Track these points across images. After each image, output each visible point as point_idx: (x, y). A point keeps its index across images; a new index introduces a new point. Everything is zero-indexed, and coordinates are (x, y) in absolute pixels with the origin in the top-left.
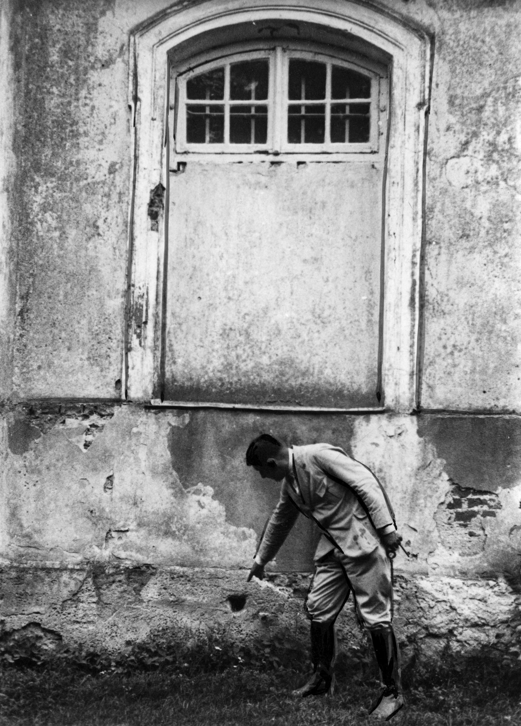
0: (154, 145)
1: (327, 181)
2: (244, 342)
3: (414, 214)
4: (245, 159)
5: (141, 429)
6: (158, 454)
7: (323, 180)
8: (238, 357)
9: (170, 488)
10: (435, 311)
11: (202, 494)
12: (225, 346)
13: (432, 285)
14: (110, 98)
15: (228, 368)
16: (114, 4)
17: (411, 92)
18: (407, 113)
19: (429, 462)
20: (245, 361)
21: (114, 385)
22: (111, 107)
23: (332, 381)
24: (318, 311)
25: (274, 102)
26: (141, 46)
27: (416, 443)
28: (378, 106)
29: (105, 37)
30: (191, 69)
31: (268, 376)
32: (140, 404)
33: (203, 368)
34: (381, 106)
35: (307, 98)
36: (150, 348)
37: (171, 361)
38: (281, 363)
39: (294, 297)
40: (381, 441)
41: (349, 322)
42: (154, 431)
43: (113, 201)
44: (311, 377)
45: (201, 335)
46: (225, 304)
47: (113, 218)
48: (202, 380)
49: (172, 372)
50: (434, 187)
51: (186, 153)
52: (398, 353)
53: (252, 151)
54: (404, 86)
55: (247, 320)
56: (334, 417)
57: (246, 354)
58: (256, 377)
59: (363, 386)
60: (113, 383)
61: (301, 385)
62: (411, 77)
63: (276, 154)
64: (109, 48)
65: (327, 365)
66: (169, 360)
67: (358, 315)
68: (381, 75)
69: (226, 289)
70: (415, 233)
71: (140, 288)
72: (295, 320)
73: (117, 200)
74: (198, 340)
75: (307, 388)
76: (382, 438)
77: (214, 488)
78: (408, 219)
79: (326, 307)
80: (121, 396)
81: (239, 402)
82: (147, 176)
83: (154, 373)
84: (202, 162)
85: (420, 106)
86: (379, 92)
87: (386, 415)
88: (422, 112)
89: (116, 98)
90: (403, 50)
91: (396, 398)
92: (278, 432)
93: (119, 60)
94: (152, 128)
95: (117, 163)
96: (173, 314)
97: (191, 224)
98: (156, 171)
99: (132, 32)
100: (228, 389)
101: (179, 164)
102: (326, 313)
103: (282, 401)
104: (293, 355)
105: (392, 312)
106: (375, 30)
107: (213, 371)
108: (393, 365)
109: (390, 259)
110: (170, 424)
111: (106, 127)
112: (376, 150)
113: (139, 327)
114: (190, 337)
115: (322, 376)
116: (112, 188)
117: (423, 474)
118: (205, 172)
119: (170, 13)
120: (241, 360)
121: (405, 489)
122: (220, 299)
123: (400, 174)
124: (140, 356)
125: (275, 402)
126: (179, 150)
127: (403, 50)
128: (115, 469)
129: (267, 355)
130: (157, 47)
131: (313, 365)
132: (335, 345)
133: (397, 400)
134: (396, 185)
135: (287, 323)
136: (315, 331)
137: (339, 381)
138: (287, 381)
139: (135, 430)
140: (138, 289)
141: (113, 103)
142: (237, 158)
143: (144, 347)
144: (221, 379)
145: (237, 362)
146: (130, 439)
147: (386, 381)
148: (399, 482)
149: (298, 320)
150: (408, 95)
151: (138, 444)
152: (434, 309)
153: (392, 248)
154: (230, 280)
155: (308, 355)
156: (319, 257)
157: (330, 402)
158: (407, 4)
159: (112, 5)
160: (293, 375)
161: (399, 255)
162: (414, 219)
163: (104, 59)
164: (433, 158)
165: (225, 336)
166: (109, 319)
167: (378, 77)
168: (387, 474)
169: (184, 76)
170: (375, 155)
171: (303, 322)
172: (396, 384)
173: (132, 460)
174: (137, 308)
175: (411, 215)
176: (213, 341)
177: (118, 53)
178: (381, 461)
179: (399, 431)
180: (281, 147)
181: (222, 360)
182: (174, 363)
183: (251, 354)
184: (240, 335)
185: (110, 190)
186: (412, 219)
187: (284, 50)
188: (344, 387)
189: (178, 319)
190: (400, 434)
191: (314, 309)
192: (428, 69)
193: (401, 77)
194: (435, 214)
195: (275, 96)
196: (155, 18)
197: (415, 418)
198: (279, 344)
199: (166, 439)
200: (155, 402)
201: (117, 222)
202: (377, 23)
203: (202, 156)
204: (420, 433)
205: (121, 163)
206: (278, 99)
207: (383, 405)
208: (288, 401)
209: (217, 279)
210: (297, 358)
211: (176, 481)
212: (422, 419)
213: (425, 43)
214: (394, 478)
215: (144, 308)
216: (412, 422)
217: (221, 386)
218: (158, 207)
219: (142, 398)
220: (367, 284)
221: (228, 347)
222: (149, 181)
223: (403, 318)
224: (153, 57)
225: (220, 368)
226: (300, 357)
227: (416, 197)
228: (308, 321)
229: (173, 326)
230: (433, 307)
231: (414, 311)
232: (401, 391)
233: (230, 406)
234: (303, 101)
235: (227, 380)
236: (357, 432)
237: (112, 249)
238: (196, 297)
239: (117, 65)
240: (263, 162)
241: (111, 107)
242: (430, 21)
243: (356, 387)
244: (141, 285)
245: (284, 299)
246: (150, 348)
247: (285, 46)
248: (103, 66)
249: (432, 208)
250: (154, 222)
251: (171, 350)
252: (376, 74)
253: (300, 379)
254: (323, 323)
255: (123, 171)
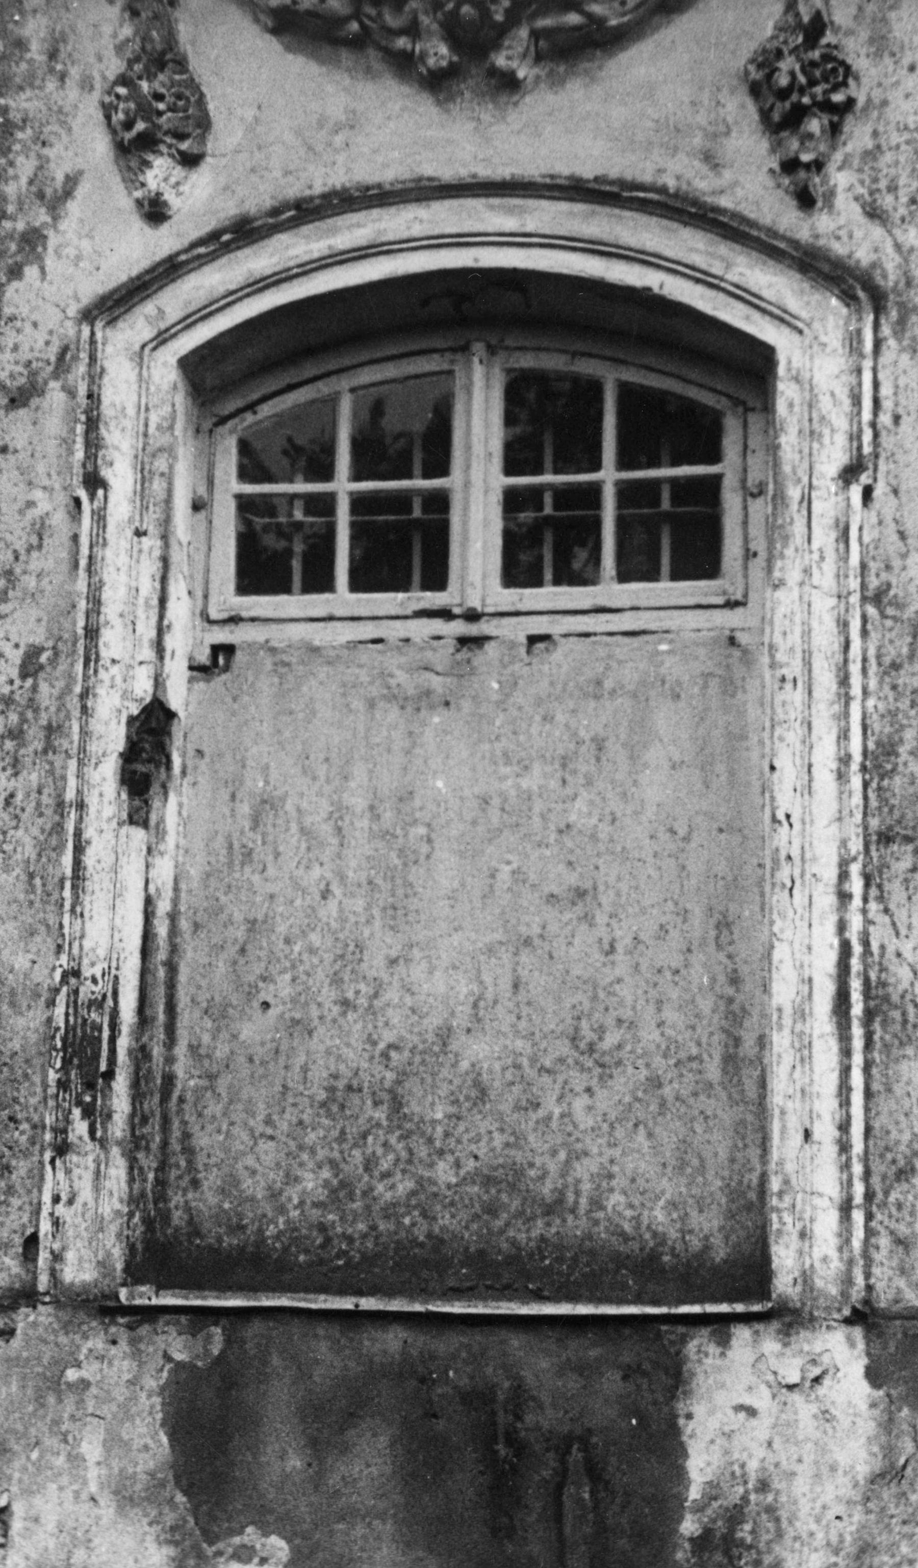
0: (141, 601)
1: (608, 684)
2: (385, 1123)
3: (840, 760)
4: (394, 631)
5: (89, 1372)
6: (137, 1443)
7: (599, 683)
8: (369, 1164)
9: (169, 1542)
10: (909, 1026)
11: (256, 1560)
12: (335, 1133)
13: (899, 955)
14: (30, 483)
15: (342, 1194)
16: (45, 249)
17: (826, 440)
18: (813, 494)
19: (902, 1461)
20: (386, 1175)
21: (20, 1250)
22: (30, 504)
23: (627, 1227)
24: (587, 1034)
25: (467, 484)
26: (109, 349)
27: (863, 1407)
28: (744, 481)
29: (18, 331)
30: (251, 407)
31: (453, 1216)
32: (87, 1300)
33: (274, 1195)
34: (750, 483)
35: (556, 471)
36: (119, 1143)
37: (187, 1179)
38: (488, 1181)
39: (522, 996)
40: (762, 1400)
41: (672, 1062)
42: (127, 1376)
43: (31, 749)
44: (570, 1218)
45: (269, 1106)
46: (334, 1021)
47: (28, 795)
48: (271, 1231)
49: (188, 1208)
50: (894, 687)
51: (234, 620)
52: (807, 1147)
53: (409, 612)
54: (807, 424)
55: (393, 1064)
56: (627, 1332)
57: (391, 1157)
58: (419, 1219)
59: (717, 1241)
60: (18, 1240)
61: (542, 1239)
62: (825, 403)
63: (472, 616)
64: (28, 356)
65: (614, 1183)
66: (180, 1177)
67: (699, 1044)
68: (750, 404)
69: (336, 980)
70: (845, 812)
71: (94, 981)
72: (525, 1062)
73: (39, 745)
74: (260, 1117)
75: (560, 1247)
76: (765, 1392)
77: (289, 1541)
78: (825, 778)
79: (610, 1021)
80: (35, 1278)
81: (372, 1291)
82: (118, 680)
83: (131, 1215)
84: (274, 644)
85: (849, 474)
86: (746, 447)
87: (775, 1325)
88: (856, 493)
89: (46, 482)
90: (801, 332)
91: (804, 1273)
92: (472, 1378)
93: (53, 384)
94: (135, 555)
95: (42, 649)
96: (193, 1049)
97: (245, 809)
98: (144, 667)
99: (88, 315)
100: (341, 1254)
101: (216, 649)
102: (611, 1040)
103: (488, 1287)
104: (519, 1156)
105: (786, 1032)
106: (723, 285)
107: (302, 1203)
108: (794, 1181)
109: (777, 890)
110: (167, 1358)
111: (17, 558)
112: (739, 596)
113: (90, 1086)
114: (238, 1116)
115: (601, 1215)
116: (30, 715)
117: (887, 1494)
118: (284, 670)
119: (187, 262)
120: (376, 1174)
121: (834, 1539)
122: (319, 1005)
123: (799, 655)
124: (92, 1166)
125: (471, 1289)
126: (214, 614)
127: (801, 332)
128: (14, 1489)
129: (450, 1158)
130: (154, 349)
131: (578, 1181)
132: (636, 1125)
133: (806, 1278)
134: (789, 686)
135: (504, 1069)
136: (579, 1089)
137: (649, 1227)
138: (502, 1231)
139: (72, 1375)
140: (88, 983)
141: (38, 495)
142: (368, 631)
143: (103, 1143)
144: (322, 1228)
145: (366, 1178)
146: (60, 1401)
147: (775, 1226)
148: (818, 1520)
149: (533, 1060)
150: (816, 445)
151: (79, 1414)
152: (905, 1022)
153: (783, 854)
154: (349, 957)
155: (562, 1155)
156: (588, 885)
157: (624, 1287)
158: (810, 216)
159: (40, 249)
160: (520, 1214)
161: (802, 875)
162: (841, 777)
163: (16, 384)
164: (890, 611)
165: (335, 1108)
166: (12, 1069)
167: (740, 409)
168: (783, 1499)
169: (230, 424)
170: (740, 610)
171: (548, 1063)
172: (803, 1235)
173: (60, 1461)
174: (83, 1038)
175: (834, 766)
176: (301, 1123)
177: (50, 369)
178: (763, 1460)
179: (816, 1371)
180: (483, 600)
181: (326, 1174)
182: (195, 1184)
183: (404, 1154)
184: (376, 1104)
185: (23, 720)
186: (834, 776)
187: (492, 350)
188: (663, 1243)
189: (206, 1062)
190: (817, 1380)
191: (577, 1029)
192: (867, 377)
193: (797, 401)
194: (900, 760)
195: (468, 467)
196: (147, 278)
197: (858, 1332)
198: (484, 1126)
199: (157, 1400)
200: (131, 1296)
201: (39, 804)
202: (728, 267)
203: (274, 627)
204: (874, 1376)
205: (54, 648)
206: (476, 475)
207: (769, 1299)
208: (507, 1287)
209: (312, 951)
210: (531, 1165)
211: (185, 1521)
212: (880, 1335)
213: (859, 311)
214: (804, 1507)
215: (106, 1034)
216: (852, 1344)
217: (323, 1246)
218: (149, 761)
219: (96, 1283)
220: (722, 956)
221: (342, 1137)
222: (125, 695)
223: (818, 1046)
224: (140, 374)
225: (322, 1195)
226: (538, 1161)
227: (846, 715)
228: (561, 1060)
229: (192, 1083)
230: (904, 1014)
231: (849, 1027)
232: (817, 1253)
233: (346, 1303)
234: (548, 478)
235: (339, 1230)
236: (693, 1374)
237: (24, 877)
238: (256, 1004)
239: (48, 396)
240: (439, 638)
241: (30, 504)
242: (873, 257)
243: (696, 1244)
244: (97, 971)
245: (495, 1002)
246: (119, 1143)
247: (494, 342)
248: (13, 400)
249: (892, 745)
250: (137, 803)
251: (189, 1151)
252: (737, 402)
253: (540, 1223)
254: (602, 1066)
255: (57, 673)
